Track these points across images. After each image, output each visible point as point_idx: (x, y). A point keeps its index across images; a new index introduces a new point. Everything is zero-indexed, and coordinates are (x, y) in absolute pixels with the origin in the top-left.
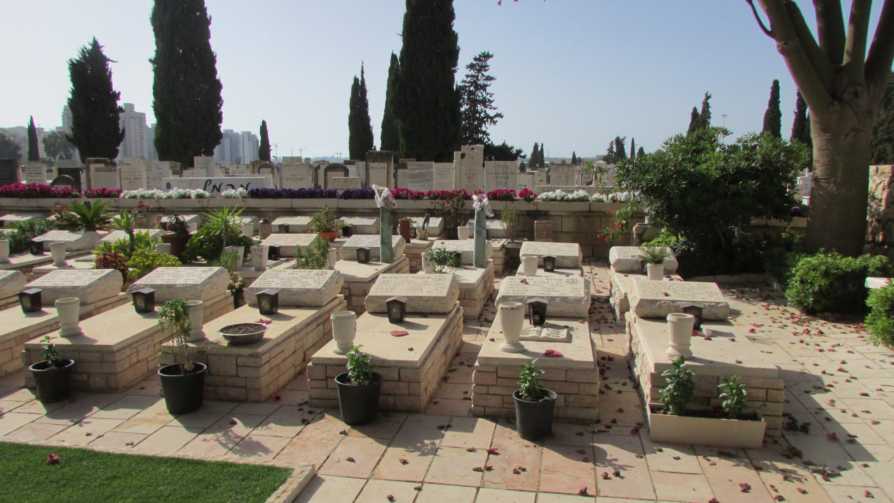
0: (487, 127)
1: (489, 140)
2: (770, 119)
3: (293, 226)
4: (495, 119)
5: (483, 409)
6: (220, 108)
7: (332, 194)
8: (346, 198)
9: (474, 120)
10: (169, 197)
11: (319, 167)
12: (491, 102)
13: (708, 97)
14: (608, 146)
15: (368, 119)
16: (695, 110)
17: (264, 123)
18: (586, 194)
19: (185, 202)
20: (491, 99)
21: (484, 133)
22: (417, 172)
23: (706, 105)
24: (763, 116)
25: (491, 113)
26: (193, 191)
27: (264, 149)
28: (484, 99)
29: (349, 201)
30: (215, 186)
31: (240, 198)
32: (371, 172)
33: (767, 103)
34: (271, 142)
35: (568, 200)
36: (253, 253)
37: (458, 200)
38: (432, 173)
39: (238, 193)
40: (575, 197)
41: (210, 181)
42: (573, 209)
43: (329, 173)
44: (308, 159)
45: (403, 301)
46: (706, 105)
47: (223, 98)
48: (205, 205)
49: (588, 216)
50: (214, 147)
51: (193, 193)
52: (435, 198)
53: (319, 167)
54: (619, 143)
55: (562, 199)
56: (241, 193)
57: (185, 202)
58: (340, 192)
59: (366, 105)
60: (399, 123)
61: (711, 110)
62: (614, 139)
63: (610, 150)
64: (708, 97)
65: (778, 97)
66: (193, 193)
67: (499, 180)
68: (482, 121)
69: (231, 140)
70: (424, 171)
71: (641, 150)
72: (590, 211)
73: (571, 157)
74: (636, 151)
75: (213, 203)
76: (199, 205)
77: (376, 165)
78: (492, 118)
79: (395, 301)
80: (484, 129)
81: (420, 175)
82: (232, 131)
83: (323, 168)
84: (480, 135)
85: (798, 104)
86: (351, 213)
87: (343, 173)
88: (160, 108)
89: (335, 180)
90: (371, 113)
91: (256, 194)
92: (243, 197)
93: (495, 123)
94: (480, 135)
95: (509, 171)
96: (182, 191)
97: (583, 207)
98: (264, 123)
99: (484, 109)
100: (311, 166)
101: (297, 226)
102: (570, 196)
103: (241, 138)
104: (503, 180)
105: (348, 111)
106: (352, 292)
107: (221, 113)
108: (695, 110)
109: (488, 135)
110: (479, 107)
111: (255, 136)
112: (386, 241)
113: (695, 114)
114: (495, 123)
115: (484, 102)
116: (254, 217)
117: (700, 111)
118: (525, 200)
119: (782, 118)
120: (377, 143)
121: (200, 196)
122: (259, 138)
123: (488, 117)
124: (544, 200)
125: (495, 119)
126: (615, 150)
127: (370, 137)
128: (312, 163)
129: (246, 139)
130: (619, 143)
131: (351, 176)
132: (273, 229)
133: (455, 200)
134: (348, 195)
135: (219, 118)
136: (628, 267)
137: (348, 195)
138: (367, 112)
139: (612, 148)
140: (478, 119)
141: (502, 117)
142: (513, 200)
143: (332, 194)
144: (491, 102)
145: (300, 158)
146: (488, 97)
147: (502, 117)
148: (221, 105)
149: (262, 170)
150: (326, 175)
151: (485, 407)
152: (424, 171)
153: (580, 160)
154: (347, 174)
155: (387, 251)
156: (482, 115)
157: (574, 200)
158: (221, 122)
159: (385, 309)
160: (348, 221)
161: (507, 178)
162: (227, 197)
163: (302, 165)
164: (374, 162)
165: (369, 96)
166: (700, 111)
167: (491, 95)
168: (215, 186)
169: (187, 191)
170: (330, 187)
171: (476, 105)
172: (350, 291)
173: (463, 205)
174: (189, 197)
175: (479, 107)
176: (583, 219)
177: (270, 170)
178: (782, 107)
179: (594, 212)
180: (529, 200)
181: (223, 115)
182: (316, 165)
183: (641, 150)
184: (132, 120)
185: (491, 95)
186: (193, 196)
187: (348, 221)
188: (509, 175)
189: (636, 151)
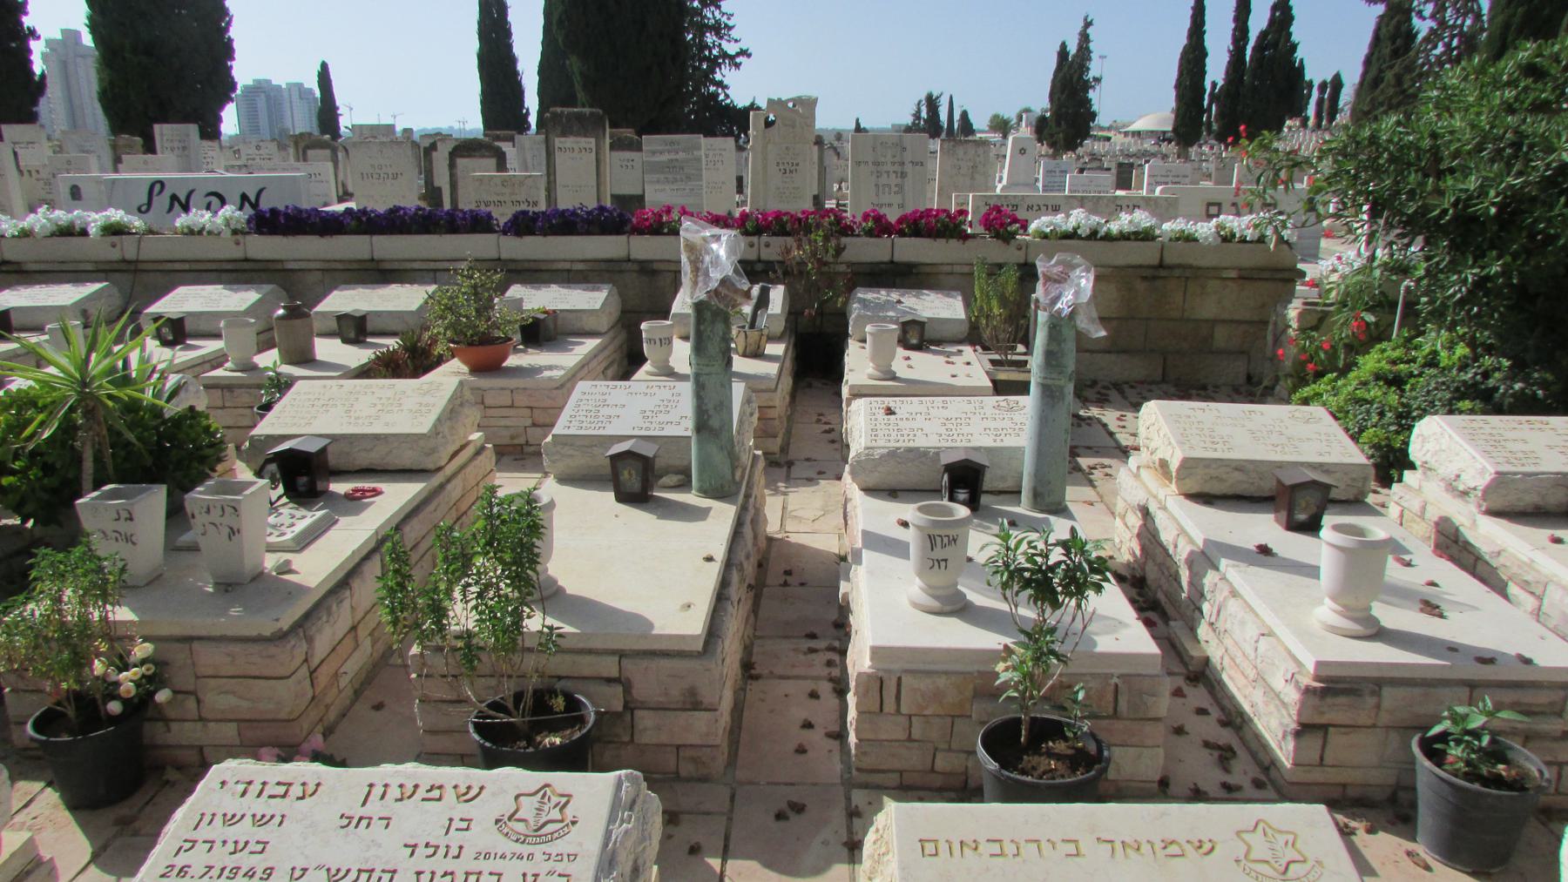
0: (725, 74)
1: (727, 96)
2: (1189, 62)
3: (378, 314)
4: (738, 60)
5: (896, 776)
6: (227, 29)
7: (479, 223)
8: (519, 234)
9: (701, 62)
10: (26, 234)
11: (433, 147)
12: (730, 28)
13: (1088, 24)
14: (913, 109)
15: (513, 60)
16: (1063, 46)
17: (324, 66)
18: (1095, 219)
19: (71, 248)
20: (730, 23)
21: (720, 84)
22: (665, 158)
23: (1084, 38)
24: (1178, 56)
25: (731, 49)
26: (94, 216)
27: (327, 112)
28: (718, 22)
29: (529, 239)
30: (174, 198)
31: (227, 234)
32: (559, 158)
33: (1185, 34)
34: (340, 99)
35: (1108, 237)
36: (200, 520)
37: (826, 239)
38: (699, 160)
39: (219, 220)
40: (1127, 229)
41: (162, 183)
42: (1120, 261)
43: (461, 162)
44: (408, 131)
45: (648, 450)
46: (1084, 38)
47: (232, 11)
48: (131, 254)
49: (1155, 278)
50: (222, 107)
51: (95, 220)
52: (758, 231)
53: (433, 147)
54: (932, 102)
55: (1093, 235)
56: (227, 222)
57: (72, 246)
58: (502, 216)
59: (507, 33)
60: (574, 64)
61: (1092, 46)
62: (923, 96)
63: (917, 116)
64: (1088, 24)
65: (1203, 23)
66: (95, 220)
67: (884, 180)
68: (714, 63)
69: (268, 98)
70: (681, 155)
71: (964, 115)
72: (1161, 266)
73: (853, 126)
74: (957, 117)
75: (152, 250)
76: (115, 255)
77: (569, 142)
78: (732, 58)
79: (628, 455)
80: (718, 77)
81: (671, 166)
82: (269, 82)
83: (450, 146)
84: (712, 89)
85: (1234, 35)
86: (535, 274)
87: (493, 162)
88: (94, 27)
89: (481, 180)
90: (518, 49)
91: (268, 222)
92: (235, 232)
93: (738, 66)
94: (712, 89)
95: (908, 157)
96: (61, 216)
97: (1144, 255)
98: (324, 66)
99: (718, 42)
100: (415, 145)
101: (390, 313)
102: (1114, 227)
103: (286, 95)
104: (894, 180)
105: (474, 45)
106: (639, 692)
107: (231, 40)
108: (1063, 46)
109: (725, 87)
110: (710, 38)
111: (311, 91)
112: (715, 422)
113: (1063, 53)
114: (738, 66)
115: (717, 29)
116: (268, 288)
117: (1072, 49)
118: (997, 236)
119: (1208, 60)
120: (532, 102)
121: (114, 231)
122: (318, 94)
123: (724, 55)
124: (1045, 236)
125: (738, 60)
126: (924, 115)
127: (519, 92)
128: (416, 137)
129: (295, 96)
130: (932, 102)
131: (514, 169)
132: (317, 325)
133: (818, 237)
134: (523, 225)
135: (227, 50)
136: (1530, 500)
137: (523, 225)
138: (510, 47)
139: (919, 111)
140: (708, 59)
141: (749, 56)
142: (965, 237)
143: (479, 223)
144: (730, 28)
145: (391, 128)
146: (724, 19)
147: (749, 56)
148: (229, 24)
149: (310, 152)
150: (452, 166)
151: (901, 772)
152: (681, 155)
153: (865, 130)
154: (502, 164)
155: (719, 458)
156: (715, 52)
157: (1123, 237)
158: (233, 59)
159: (607, 469)
160: (537, 299)
161: (903, 175)
162: (191, 232)
163: (396, 143)
164: (564, 134)
165: (512, 17)
166: (1072, 49)
167: (730, 16)
168: (174, 198)
169: (77, 215)
170: (466, 204)
171: (703, 34)
172: (627, 686)
173: (839, 250)
174: (84, 233)
175: (710, 38)
176: (1141, 286)
177: (328, 152)
178: (1209, 42)
179: (1171, 267)
180: (1007, 238)
181: (236, 45)
182: (426, 143)
183: (964, 115)
184: (79, 60)
185: (730, 16)
186: (93, 230)
187: (537, 299)
188: (908, 168)
189: (957, 117)
